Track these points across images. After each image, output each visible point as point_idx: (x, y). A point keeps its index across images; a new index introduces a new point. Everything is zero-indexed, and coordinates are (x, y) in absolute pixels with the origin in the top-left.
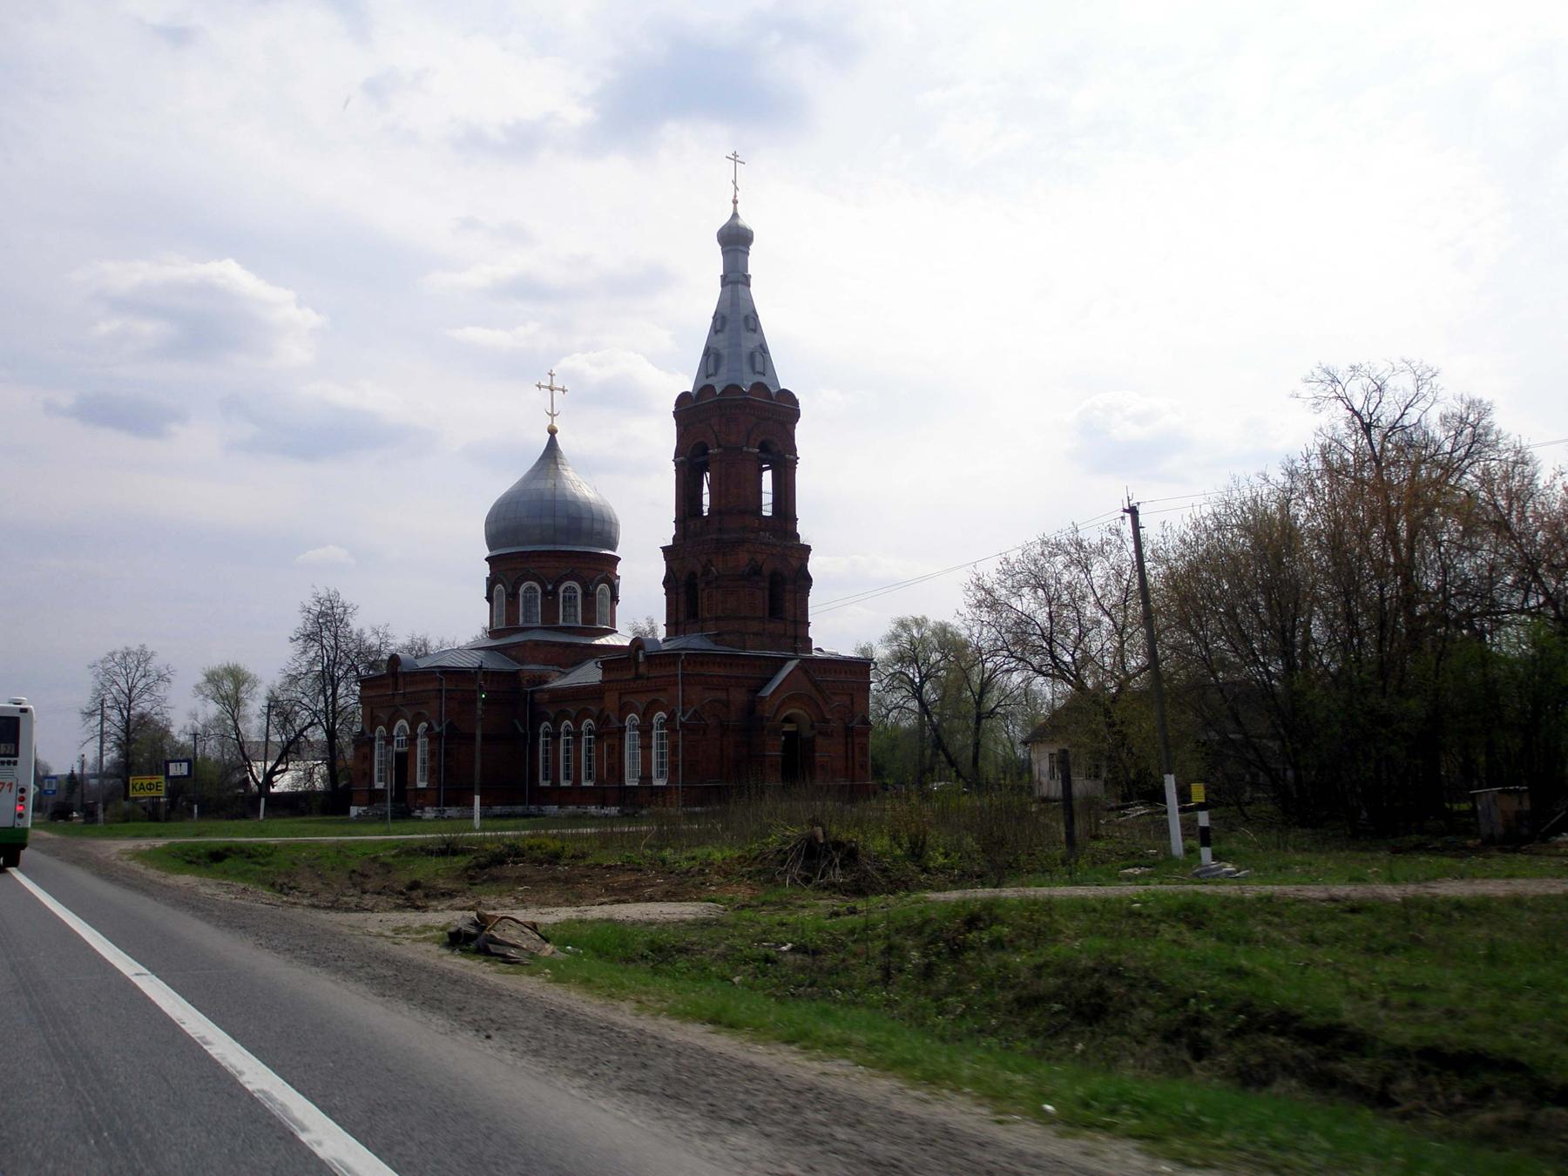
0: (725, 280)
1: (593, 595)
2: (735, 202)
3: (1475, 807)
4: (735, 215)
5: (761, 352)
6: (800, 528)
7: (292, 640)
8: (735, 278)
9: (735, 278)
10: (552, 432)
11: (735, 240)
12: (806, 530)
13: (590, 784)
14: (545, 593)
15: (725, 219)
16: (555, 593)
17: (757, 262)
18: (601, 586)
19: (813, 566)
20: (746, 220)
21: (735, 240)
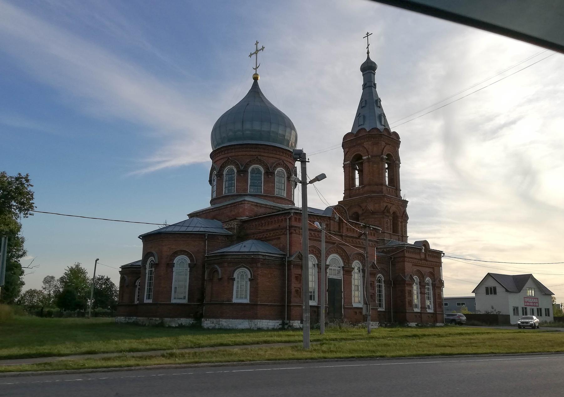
0: (364, 86)
1: (273, 173)
2: (368, 53)
3: (358, 317)
4: (368, 58)
5: (382, 117)
6: (402, 194)
7: (27, 175)
8: (369, 86)
9: (369, 86)
10: (256, 79)
11: (369, 68)
12: (404, 193)
13: (150, 301)
14: (239, 172)
15: (365, 59)
16: (245, 171)
17: (379, 77)
18: (278, 169)
19: (409, 211)
20: (372, 59)
21: (369, 68)
